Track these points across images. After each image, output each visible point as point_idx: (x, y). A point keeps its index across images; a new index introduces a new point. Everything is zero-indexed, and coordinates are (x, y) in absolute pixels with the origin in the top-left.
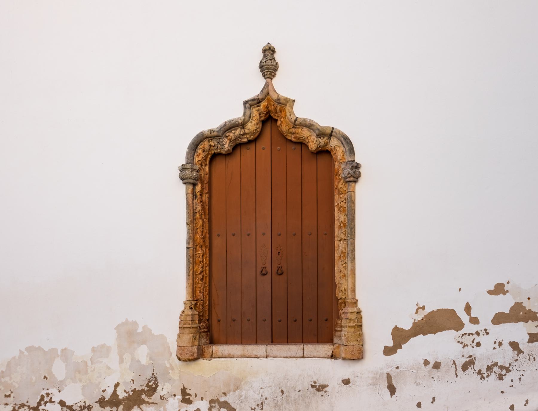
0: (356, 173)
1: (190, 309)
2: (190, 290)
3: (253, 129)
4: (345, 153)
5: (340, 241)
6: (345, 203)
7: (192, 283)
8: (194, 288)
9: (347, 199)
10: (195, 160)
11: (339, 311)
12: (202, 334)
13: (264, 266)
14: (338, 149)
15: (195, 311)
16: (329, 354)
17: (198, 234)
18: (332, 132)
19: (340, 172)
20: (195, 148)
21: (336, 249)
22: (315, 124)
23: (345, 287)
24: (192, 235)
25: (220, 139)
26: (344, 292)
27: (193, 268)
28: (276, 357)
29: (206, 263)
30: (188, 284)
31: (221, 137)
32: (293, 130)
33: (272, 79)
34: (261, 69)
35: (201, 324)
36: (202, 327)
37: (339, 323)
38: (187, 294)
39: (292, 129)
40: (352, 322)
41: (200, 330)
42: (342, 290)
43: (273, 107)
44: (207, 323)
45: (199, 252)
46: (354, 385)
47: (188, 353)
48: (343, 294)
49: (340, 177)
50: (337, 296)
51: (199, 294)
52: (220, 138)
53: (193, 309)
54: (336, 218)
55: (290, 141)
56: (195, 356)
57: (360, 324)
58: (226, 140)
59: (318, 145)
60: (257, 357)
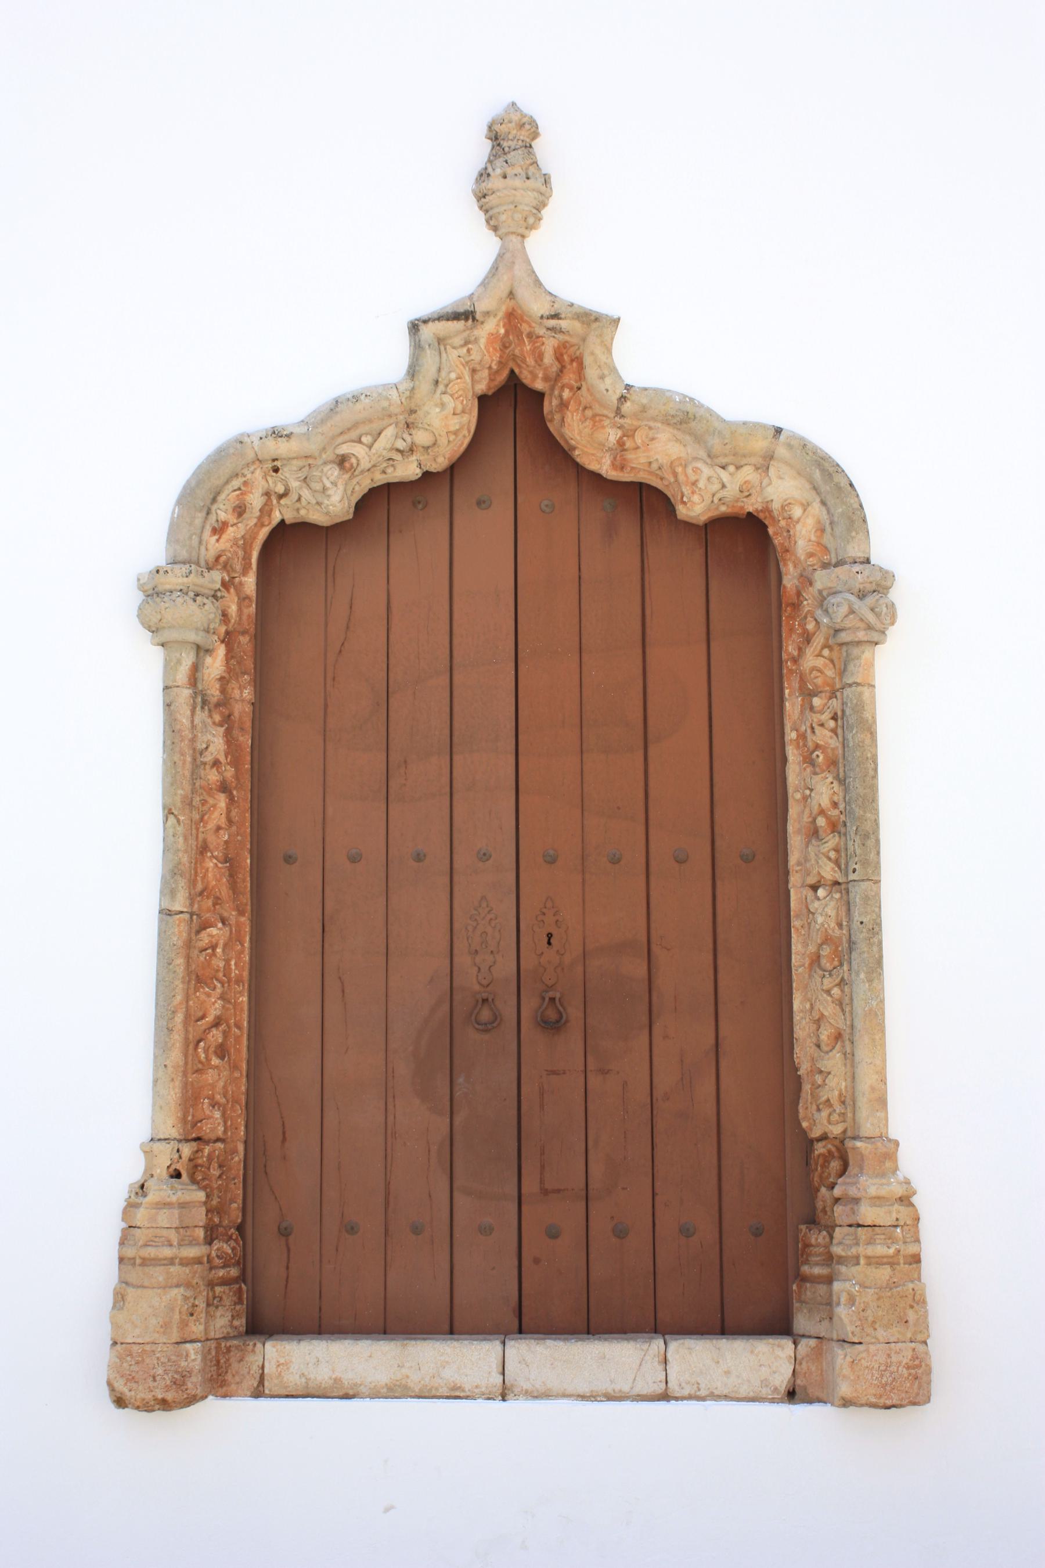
0: (876, 610)
1: (172, 1177)
2: (173, 1094)
4: (828, 529)
7: (181, 1063)
8: (189, 1087)
9: (839, 713)
11: (818, 1190)
12: (218, 1290)
14: (797, 512)
16: (777, 1383)
17: (209, 854)
20: (208, 502)
24: (185, 859)
26: (838, 1108)
27: (187, 998)
28: (545, 1395)
29: (239, 981)
30: (165, 1066)
35: (216, 1245)
36: (218, 1256)
37: (818, 1245)
41: (211, 1269)
42: (828, 1100)
44: (236, 1240)
45: (213, 931)
47: (160, 1371)
50: (805, 1124)
51: (207, 1112)
55: (597, 477)
59: (714, 495)
60: (462, 1394)
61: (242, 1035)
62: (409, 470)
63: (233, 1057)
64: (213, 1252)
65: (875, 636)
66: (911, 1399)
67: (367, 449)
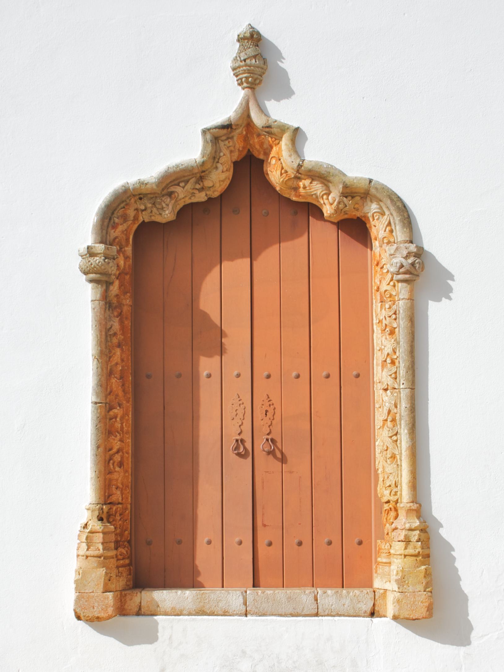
1: (99, 520)
6: (395, 319)
10: (110, 236)
12: (120, 569)
13: (238, 437)
15: (109, 524)
17: (113, 376)
19: (383, 261)
20: (110, 214)
21: (377, 406)
23: (397, 479)
44: (127, 547)
48: (393, 493)
49: (385, 271)
53: (105, 520)
54: (376, 348)
61: (129, 457)
67: (182, 189)
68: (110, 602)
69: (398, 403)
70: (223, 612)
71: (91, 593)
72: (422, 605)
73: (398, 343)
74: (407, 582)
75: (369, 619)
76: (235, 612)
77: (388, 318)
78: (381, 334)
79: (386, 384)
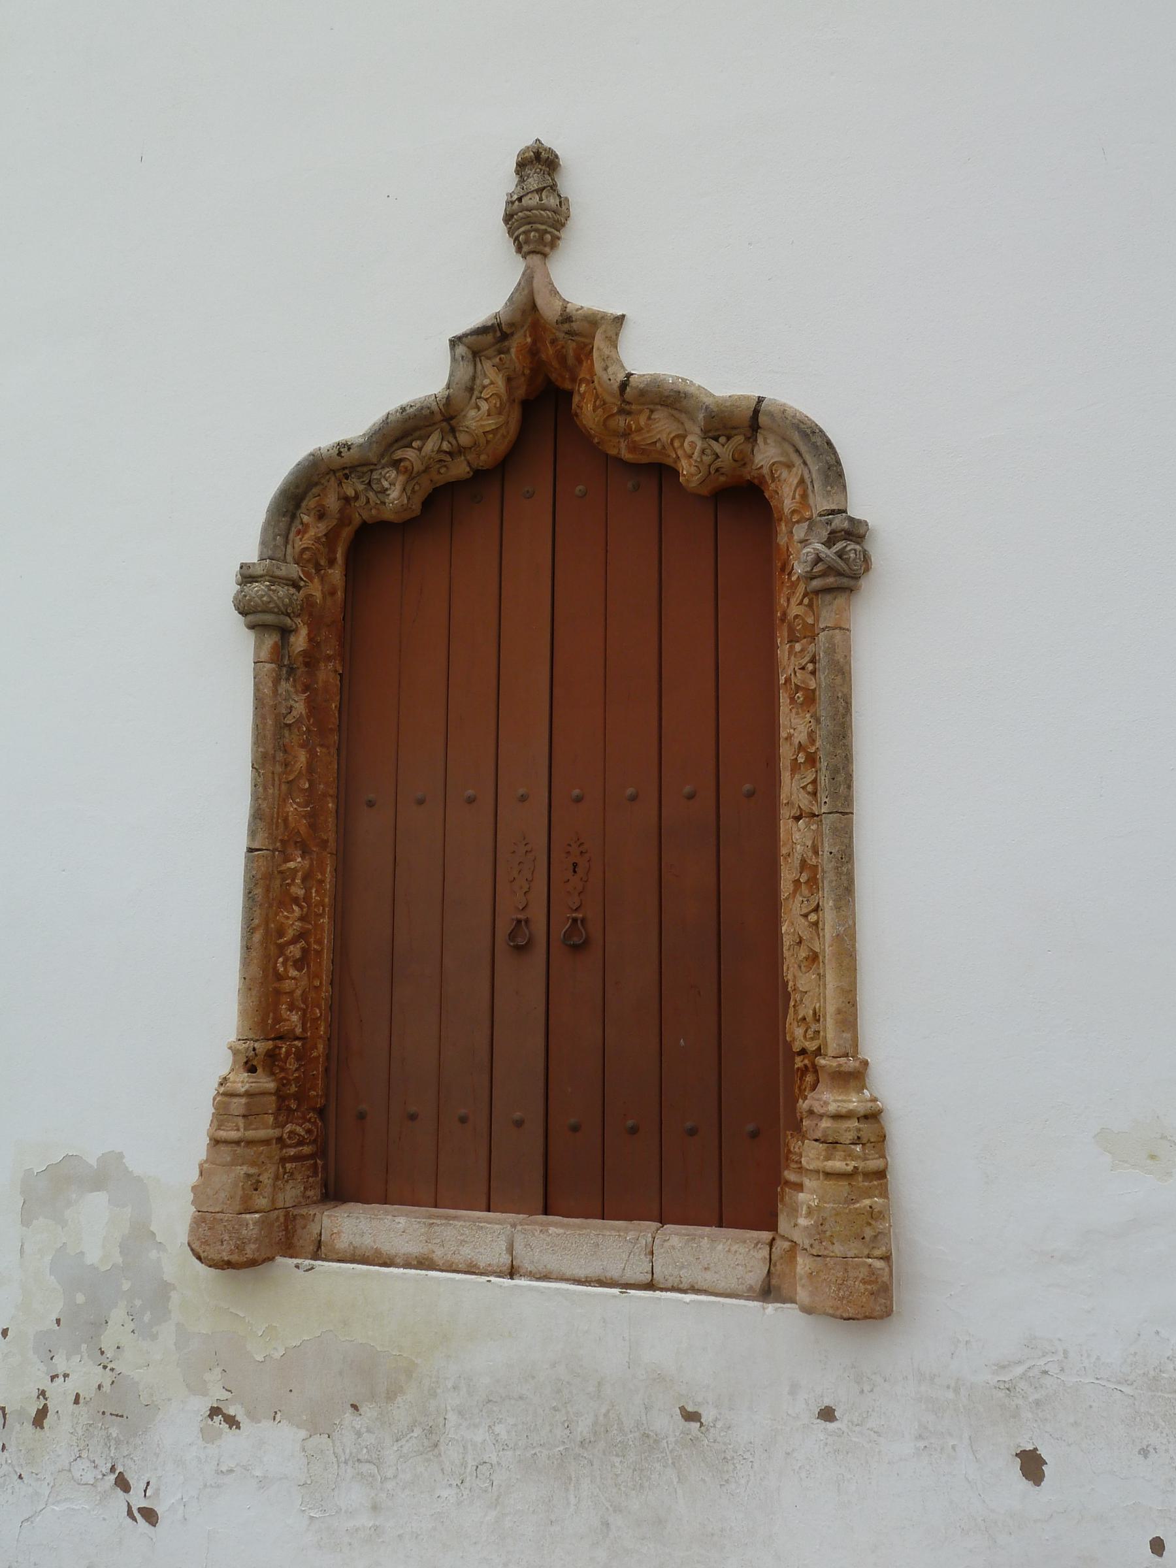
0: (845, 557)
3: (482, 431)
5: (797, 818)
6: (813, 673)
12: (288, 1166)
13: (521, 916)
14: (785, 474)
18: (756, 412)
21: (784, 851)
22: (692, 390)
23: (818, 1005)
25: (372, 471)
28: (545, 1277)
30: (245, 978)
31: (376, 465)
32: (621, 422)
33: (545, 255)
34: (508, 226)
35: (289, 1127)
36: (289, 1138)
38: (243, 1013)
39: (617, 417)
40: (839, 1154)
42: (804, 1019)
43: (551, 351)
44: (315, 1123)
46: (857, 1429)
48: (810, 1033)
52: (372, 467)
55: (619, 460)
56: (248, 1251)
57: (874, 1164)
58: (395, 472)
59: (710, 466)
61: (322, 949)
62: (460, 469)
63: (312, 968)
64: (285, 1135)
65: (845, 582)
66: (867, 1314)
67: (418, 453)
68: (250, 1233)
69: (820, 844)
70: (468, 1266)
71: (218, 1212)
72: (862, 1287)
73: (818, 721)
74: (828, 1234)
75: (757, 1304)
76: (489, 1269)
77: (799, 672)
78: (790, 705)
79: (797, 806)
